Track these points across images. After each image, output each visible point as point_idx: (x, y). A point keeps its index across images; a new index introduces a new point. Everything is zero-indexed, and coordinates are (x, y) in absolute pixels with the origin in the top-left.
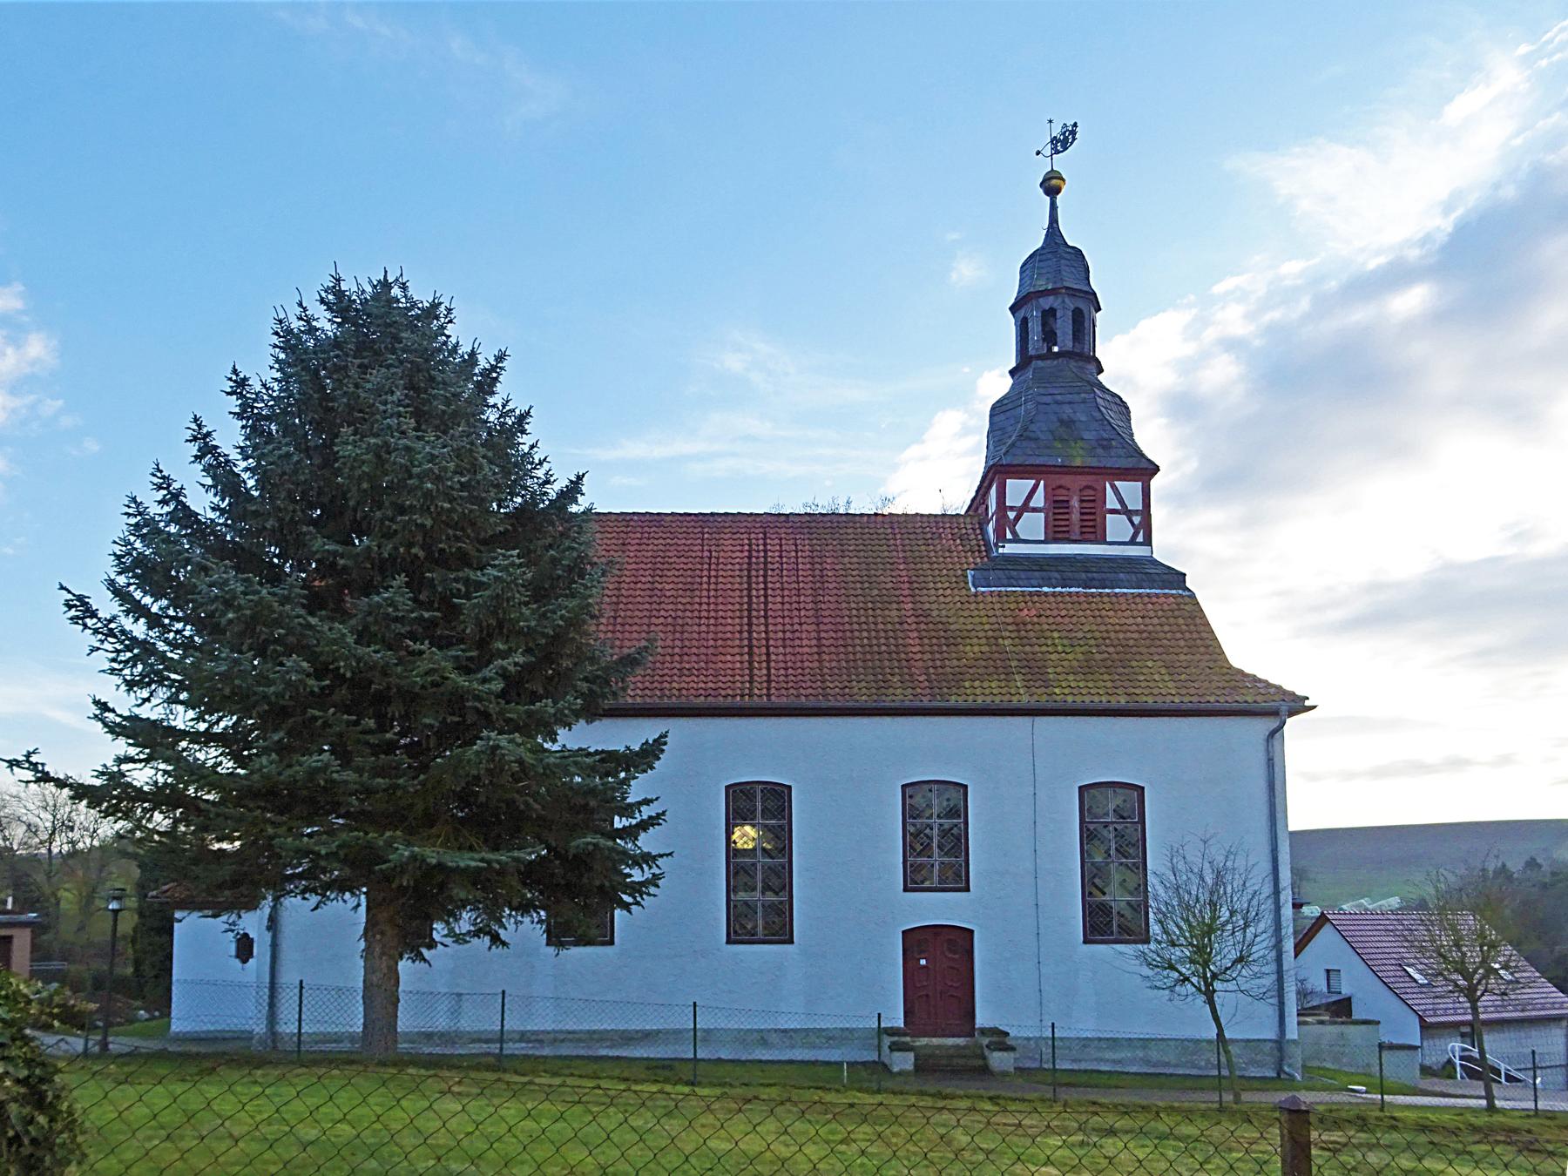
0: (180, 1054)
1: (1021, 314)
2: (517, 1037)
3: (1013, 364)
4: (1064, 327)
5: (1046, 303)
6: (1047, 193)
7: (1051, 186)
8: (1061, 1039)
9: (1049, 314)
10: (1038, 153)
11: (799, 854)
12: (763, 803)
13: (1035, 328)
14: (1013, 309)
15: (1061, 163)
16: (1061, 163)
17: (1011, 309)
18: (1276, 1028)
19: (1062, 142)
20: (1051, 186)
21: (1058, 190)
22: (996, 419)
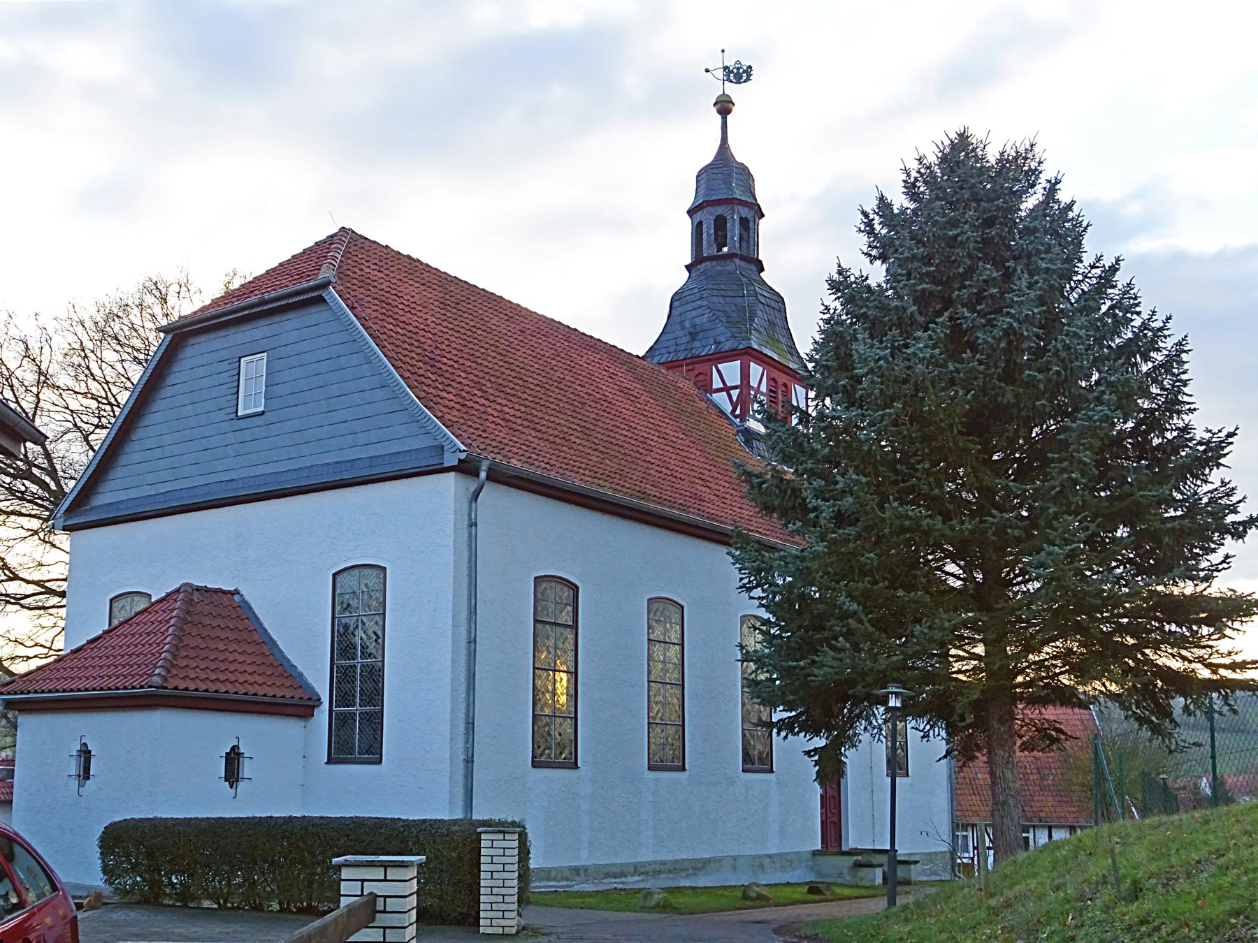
0: (623, 875)
1: (698, 217)
2: (632, 870)
3: (689, 261)
4: (734, 230)
5: (720, 210)
6: (719, 112)
7: (724, 107)
8: (547, 874)
9: (720, 223)
10: (707, 71)
11: (584, 637)
12: (664, 609)
13: (709, 230)
14: (691, 212)
15: (41, 324)
16: (733, 90)
17: (689, 212)
18: (460, 803)
19: (739, 74)
20: (724, 107)
21: (729, 111)
22: (676, 304)
